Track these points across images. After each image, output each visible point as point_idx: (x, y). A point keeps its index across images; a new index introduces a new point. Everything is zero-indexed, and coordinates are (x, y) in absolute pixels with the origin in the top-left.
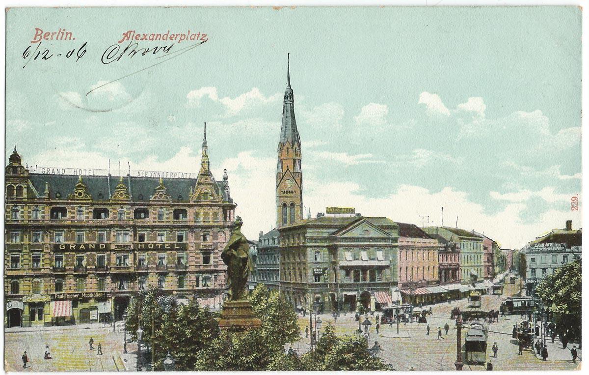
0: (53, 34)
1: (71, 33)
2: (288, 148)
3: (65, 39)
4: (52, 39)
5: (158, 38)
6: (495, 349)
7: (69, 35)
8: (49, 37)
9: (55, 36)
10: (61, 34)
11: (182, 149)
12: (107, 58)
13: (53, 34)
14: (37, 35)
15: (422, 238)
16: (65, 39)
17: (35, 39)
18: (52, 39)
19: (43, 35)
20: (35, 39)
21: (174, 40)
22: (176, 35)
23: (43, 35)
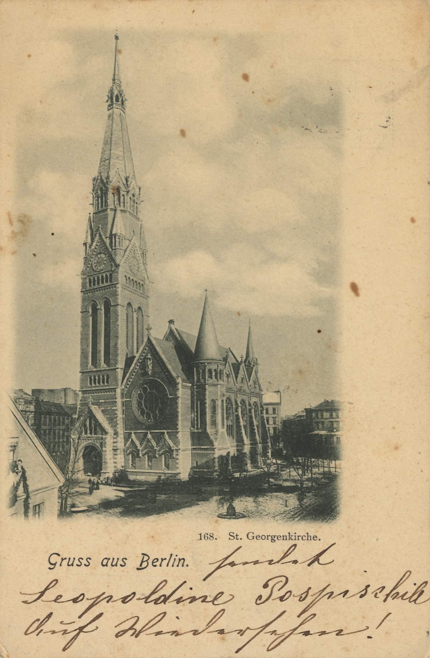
0: (162, 560)
1: (68, 565)
2: (137, 352)
3: (178, 566)
4: (160, 566)
5: (180, 565)
6: (287, 391)
7: (114, 564)
8: (158, 564)
9: (165, 563)
10: (172, 560)
11: (120, 57)
12: (138, 618)
13: (162, 560)
14: (142, 562)
15: (94, 415)
16: (178, 566)
17: (141, 565)
18: (160, 566)
19: (150, 561)
20: (141, 565)
21: (158, 567)
22: (268, 536)
23: (150, 561)
